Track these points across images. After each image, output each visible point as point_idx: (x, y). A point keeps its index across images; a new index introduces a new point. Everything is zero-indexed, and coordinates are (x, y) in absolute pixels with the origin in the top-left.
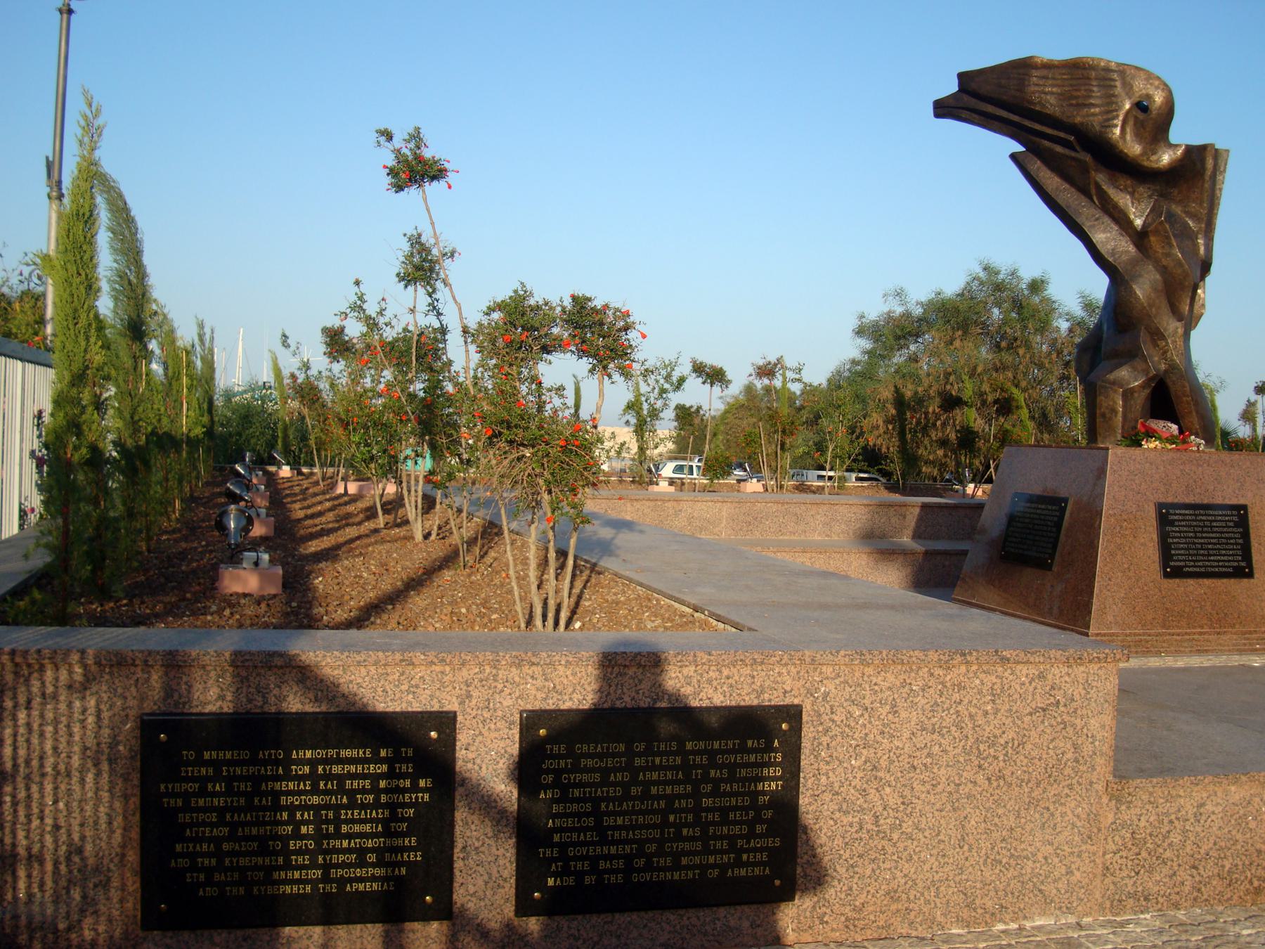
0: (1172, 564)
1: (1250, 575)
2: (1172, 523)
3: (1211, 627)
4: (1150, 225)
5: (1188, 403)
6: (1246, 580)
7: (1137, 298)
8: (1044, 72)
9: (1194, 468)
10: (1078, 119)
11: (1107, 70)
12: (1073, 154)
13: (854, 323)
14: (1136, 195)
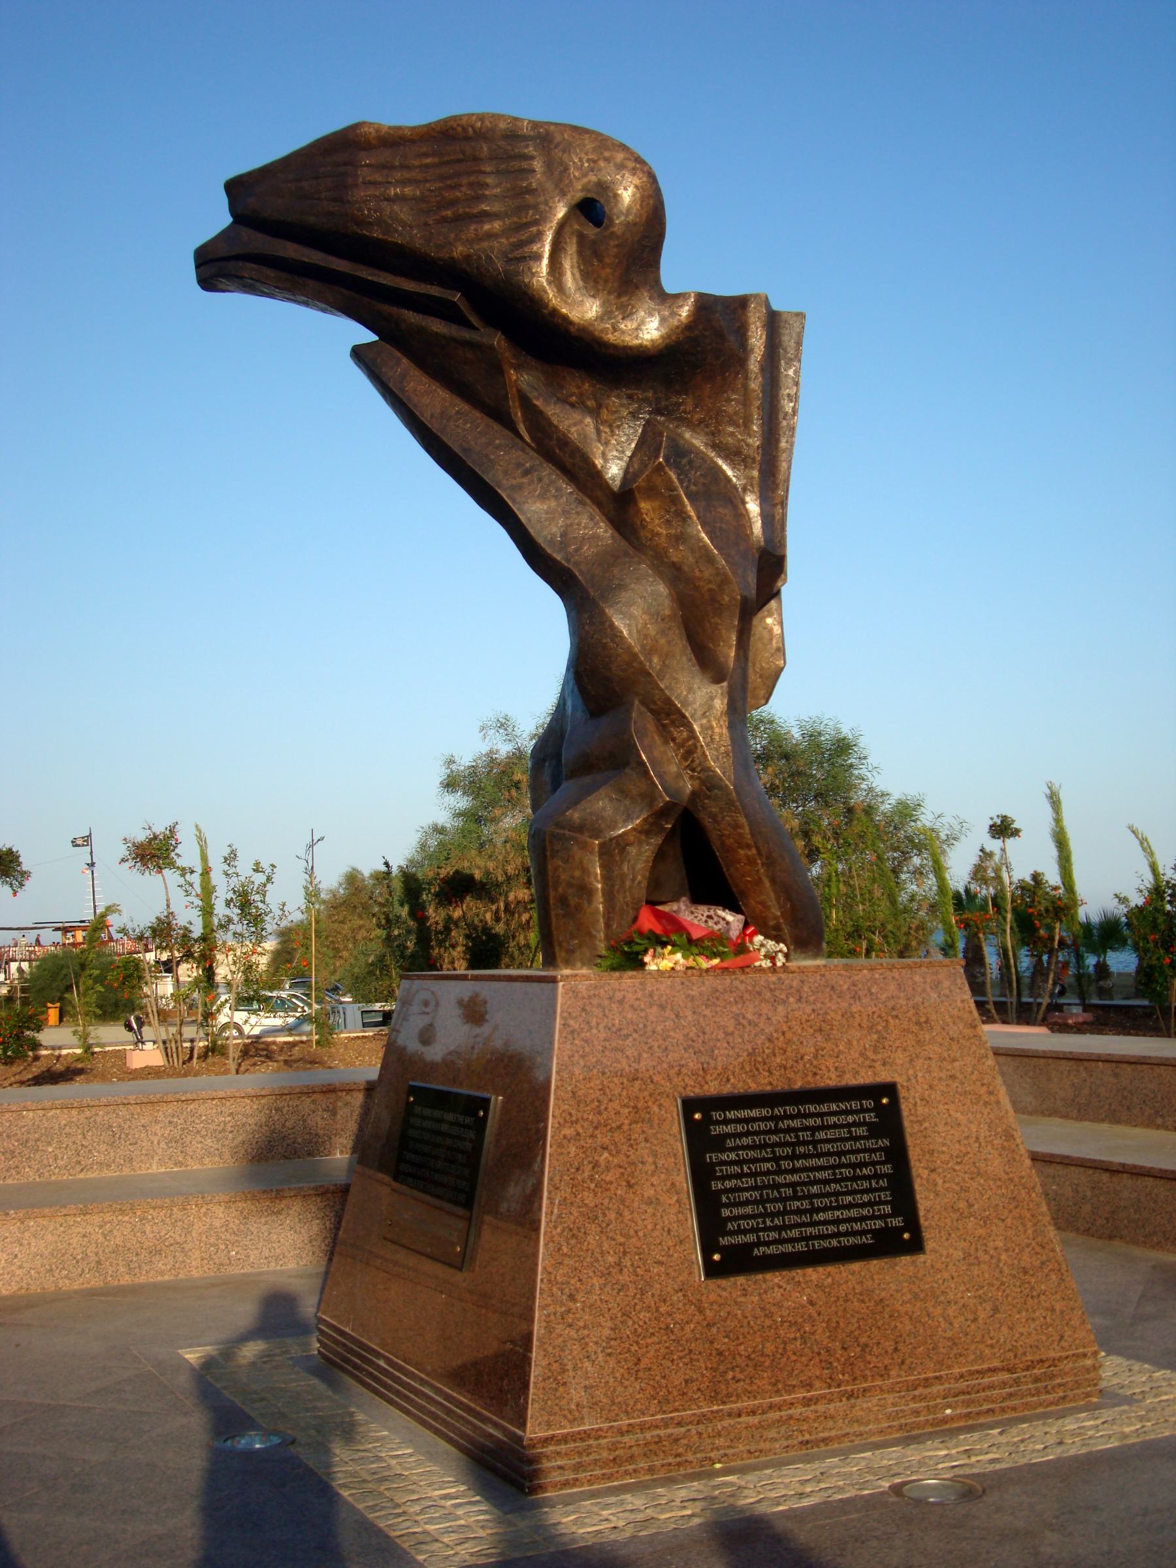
0: (724, 1241)
1: (916, 1246)
2: (719, 1144)
3: (831, 1382)
4: (636, 475)
5: (751, 861)
6: (906, 1260)
7: (616, 634)
8: (384, 155)
9: (765, 1009)
10: (459, 250)
11: (513, 135)
12: (467, 334)
13: (439, 773)
14: (605, 414)
